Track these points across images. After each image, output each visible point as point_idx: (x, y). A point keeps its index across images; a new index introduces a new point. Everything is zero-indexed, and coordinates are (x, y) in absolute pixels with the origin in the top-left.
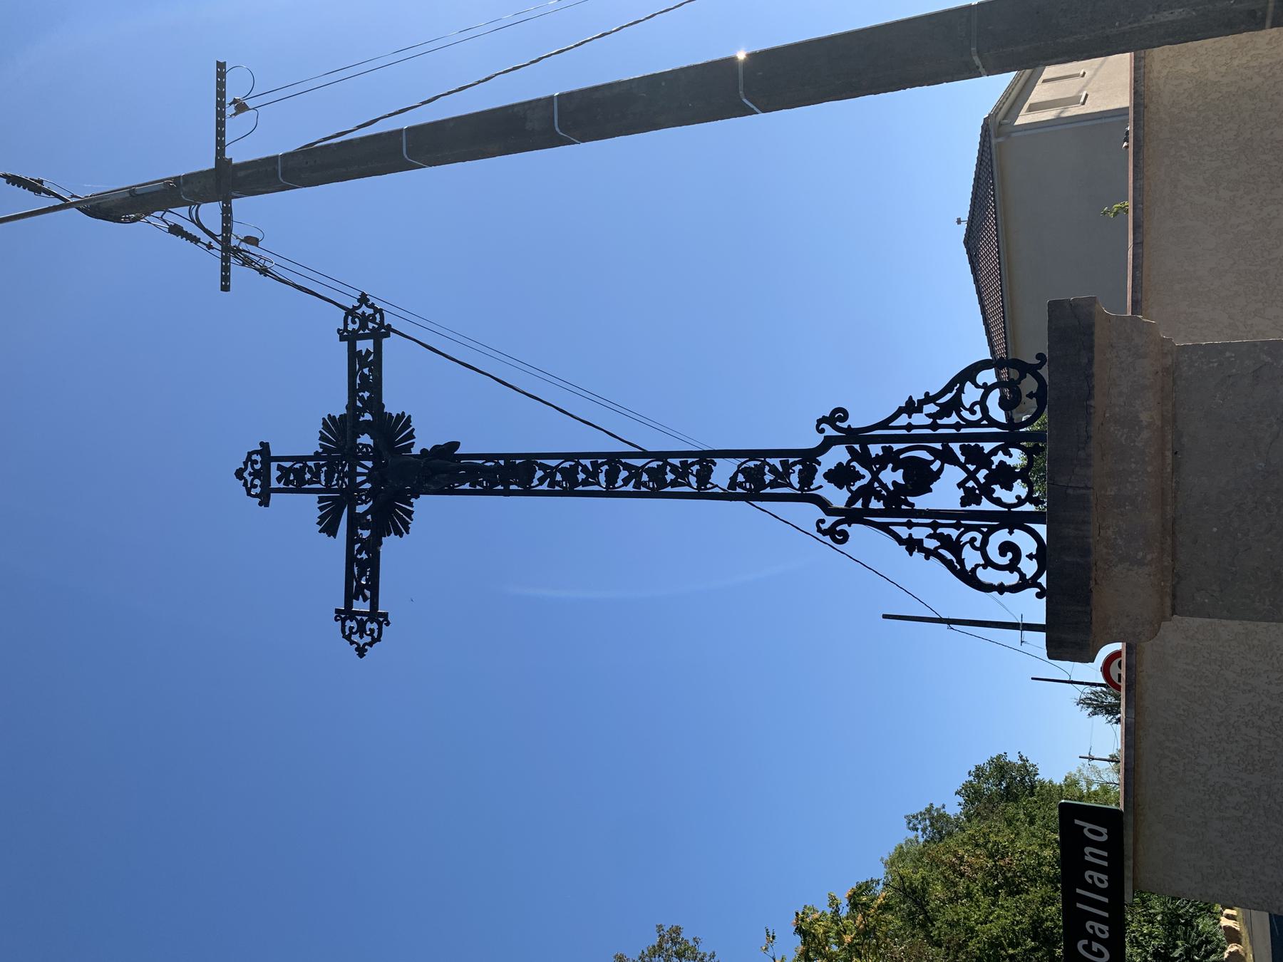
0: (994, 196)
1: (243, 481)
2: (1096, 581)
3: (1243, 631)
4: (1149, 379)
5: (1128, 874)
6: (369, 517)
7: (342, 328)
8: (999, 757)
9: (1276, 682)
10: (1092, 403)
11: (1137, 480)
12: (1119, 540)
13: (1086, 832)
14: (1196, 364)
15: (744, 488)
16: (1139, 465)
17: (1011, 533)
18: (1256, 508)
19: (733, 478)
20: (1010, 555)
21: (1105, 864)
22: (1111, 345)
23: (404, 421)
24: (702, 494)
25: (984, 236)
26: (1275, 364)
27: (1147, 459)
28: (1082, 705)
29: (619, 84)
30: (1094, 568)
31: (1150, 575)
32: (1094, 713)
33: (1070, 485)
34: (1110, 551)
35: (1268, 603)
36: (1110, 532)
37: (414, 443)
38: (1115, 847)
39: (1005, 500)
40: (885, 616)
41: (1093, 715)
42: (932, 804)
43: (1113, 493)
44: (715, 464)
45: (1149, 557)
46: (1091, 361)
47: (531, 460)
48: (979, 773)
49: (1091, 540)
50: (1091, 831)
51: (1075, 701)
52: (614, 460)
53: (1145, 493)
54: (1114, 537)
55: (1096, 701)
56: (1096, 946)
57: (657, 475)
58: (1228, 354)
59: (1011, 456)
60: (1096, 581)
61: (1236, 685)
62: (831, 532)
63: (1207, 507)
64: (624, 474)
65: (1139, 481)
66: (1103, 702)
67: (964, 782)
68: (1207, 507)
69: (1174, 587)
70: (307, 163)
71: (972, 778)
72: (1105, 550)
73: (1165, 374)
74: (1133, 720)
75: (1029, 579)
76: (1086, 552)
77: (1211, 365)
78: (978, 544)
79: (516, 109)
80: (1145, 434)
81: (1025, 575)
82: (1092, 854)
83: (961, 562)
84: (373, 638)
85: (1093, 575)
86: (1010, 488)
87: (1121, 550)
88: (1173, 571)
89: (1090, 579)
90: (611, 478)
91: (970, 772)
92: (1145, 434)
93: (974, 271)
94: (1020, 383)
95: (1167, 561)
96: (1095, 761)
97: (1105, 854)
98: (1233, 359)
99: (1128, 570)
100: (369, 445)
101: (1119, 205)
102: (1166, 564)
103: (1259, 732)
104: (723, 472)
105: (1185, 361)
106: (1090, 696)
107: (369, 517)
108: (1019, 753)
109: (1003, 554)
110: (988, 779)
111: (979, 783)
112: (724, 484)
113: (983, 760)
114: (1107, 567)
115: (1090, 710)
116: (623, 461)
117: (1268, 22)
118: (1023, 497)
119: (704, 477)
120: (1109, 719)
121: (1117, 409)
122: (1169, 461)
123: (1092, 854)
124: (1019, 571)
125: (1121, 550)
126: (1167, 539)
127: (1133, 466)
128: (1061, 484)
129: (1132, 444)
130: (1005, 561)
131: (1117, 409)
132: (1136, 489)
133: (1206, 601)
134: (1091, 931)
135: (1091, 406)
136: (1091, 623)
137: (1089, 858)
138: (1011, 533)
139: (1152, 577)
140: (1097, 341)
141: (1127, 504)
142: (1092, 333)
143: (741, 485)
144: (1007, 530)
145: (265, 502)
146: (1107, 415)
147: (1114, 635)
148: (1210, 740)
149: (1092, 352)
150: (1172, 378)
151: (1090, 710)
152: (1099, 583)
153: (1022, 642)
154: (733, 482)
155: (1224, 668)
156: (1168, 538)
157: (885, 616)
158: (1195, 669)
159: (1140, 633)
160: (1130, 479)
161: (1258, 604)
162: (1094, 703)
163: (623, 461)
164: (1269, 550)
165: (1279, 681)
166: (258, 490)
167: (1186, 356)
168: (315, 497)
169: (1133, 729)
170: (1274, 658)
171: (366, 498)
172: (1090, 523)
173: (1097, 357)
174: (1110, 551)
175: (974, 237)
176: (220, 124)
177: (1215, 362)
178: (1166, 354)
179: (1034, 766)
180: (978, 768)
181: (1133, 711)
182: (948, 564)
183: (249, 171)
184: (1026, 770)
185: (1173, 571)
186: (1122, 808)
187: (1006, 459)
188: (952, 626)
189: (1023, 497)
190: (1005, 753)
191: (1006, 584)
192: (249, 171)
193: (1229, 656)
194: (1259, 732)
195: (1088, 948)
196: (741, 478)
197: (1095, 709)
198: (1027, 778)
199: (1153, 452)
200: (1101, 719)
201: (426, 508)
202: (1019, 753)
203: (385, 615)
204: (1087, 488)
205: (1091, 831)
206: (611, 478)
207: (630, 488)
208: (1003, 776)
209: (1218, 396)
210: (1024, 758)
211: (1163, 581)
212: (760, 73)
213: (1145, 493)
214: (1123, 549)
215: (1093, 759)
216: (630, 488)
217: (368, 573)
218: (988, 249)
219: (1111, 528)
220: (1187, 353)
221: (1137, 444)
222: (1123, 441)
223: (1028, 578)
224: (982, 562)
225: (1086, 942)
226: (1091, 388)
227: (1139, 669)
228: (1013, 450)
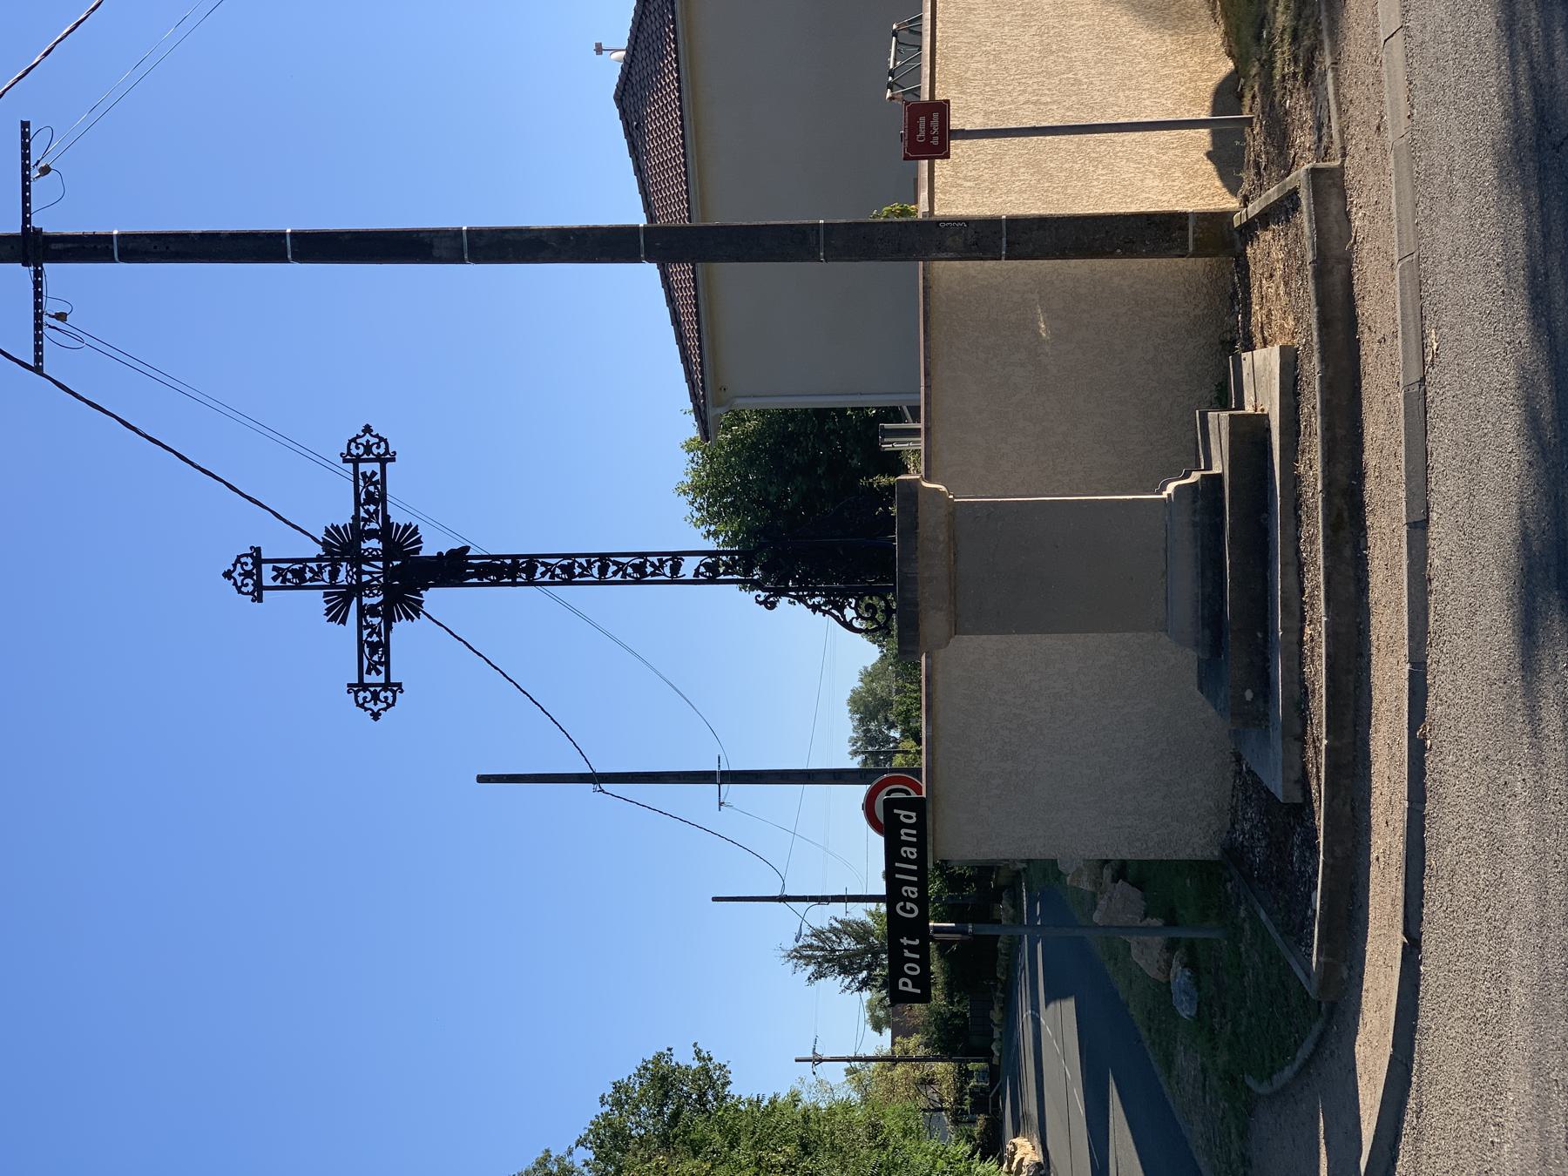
0: (675, 41)
1: (232, 580)
5: (930, 847)
6: (380, 608)
7: (345, 452)
8: (659, 1057)
10: (918, 531)
13: (902, 818)
15: (705, 576)
19: (697, 570)
21: (915, 840)
23: (412, 531)
24: (675, 580)
28: (795, 961)
29: (528, 230)
32: (819, 975)
37: (421, 547)
38: (921, 826)
40: (483, 779)
41: (817, 978)
42: (547, 1151)
44: (683, 560)
47: (532, 560)
48: (620, 1097)
50: (906, 816)
51: (783, 954)
52: (604, 558)
55: (822, 949)
56: (909, 905)
57: (639, 569)
62: (764, 603)
64: (613, 568)
66: (833, 950)
67: (594, 1119)
69: (956, 621)
70: (155, 247)
71: (607, 1108)
76: (917, 605)
78: (853, 605)
79: (421, 235)
80: (941, 546)
82: (906, 834)
83: (844, 616)
84: (388, 704)
90: (603, 570)
91: (603, 1097)
92: (941, 546)
93: (635, 150)
96: (824, 1063)
97: (914, 832)
100: (379, 549)
101: (889, 208)
104: (689, 567)
106: (810, 940)
107: (380, 608)
108: (695, 1045)
110: (637, 1107)
111: (621, 1115)
112: (690, 576)
113: (626, 1067)
115: (811, 968)
116: (612, 559)
117: (1003, 258)
119: (675, 569)
120: (847, 981)
123: (906, 834)
134: (905, 894)
137: (904, 838)
143: (702, 574)
145: (259, 599)
151: (811, 968)
153: (721, 804)
154: (697, 573)
157: (483, 779)
162: (818, 953)
163: (612, 559)
166: (250, 588)
168: (321, 592)
171: (379, 592)
176: (26, 189)
179: (722, 1067)
180: (617, 1087)
182: (836, 618)
183: (69, 245)
184: (709, 1079)
186: (924, 795)
188: (604, 786)
190: (669, 1049)
192: (69, 245)
195: (903, 909)
196: (702, 569)
197: (820, 965)
198: (710, 1092)
200: (834, 983)
201: (433, 598)
202: (695, 1045)
203: (399, 685)
205: (906, 816)
206: (603, 570)
207: (547, 578)
208: (666, 1095)
210: (704, 1054)
212: (658, 244)
215: (821, 1061)
216: (547, 578)
217: (380, 653)
224: (855, 616)
225: (902, 904)
226: (917, 523)
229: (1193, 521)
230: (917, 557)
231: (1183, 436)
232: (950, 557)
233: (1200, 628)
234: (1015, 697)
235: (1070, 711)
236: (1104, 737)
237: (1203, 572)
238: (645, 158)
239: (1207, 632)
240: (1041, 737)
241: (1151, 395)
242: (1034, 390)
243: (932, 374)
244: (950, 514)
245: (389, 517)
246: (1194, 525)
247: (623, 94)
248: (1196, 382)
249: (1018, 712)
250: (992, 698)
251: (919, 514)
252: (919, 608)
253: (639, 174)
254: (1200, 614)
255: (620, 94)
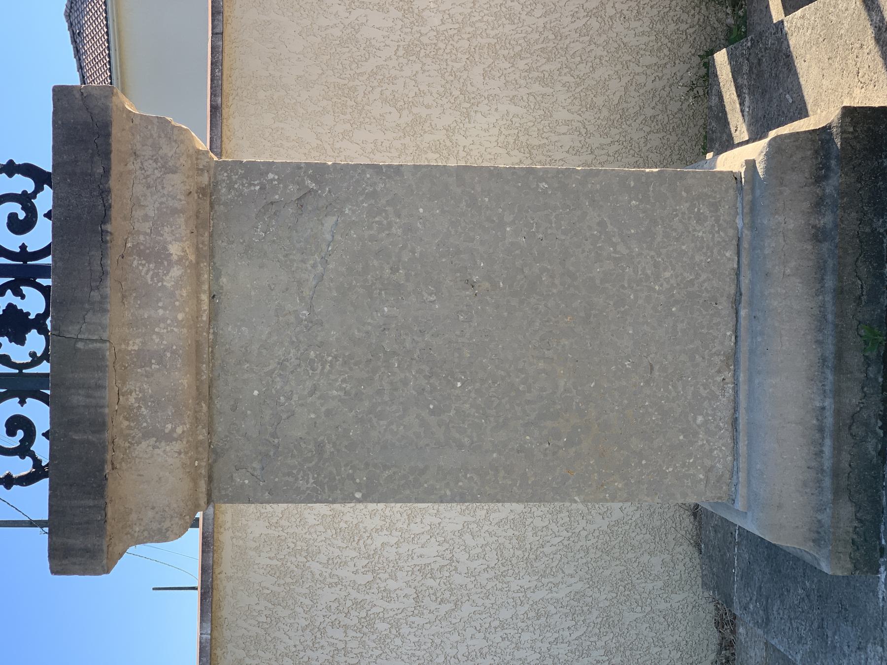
2: (113, 464)
3: (331, 513)
4: (180, 200)
9: (363, 570)
10: (108, 227)
11: (165, 330)
12: (143, 409)
14: (236, 186)
16: (168, 312)
17: (22, 402)
18: (299, 365)
20: (20, 434)
22: (135, 153)
25: (93, 7)
26: (320, 192)
27: (177, 303)
30: (110, 447)
31: (180, 453)
33: (80, 337)
34: (132, 424)
35: (311, 481)
36: (132, 400)
39: (15, 359)
43: (136, 348)
45: (179, 430)
46: (107, 172)
49: (107, 410)
53: (174, 347)
54: (137, 405)
58: (271, 176)
59: (23, 297)
60: (113, 464)
61: (321, 579)
63: (248, 365)
65: (168, 332)
68: (248, 365)
69: (210, 468)
72: (126, 423)
73: (201, 196)
74: (209, 636)
75: (45, 466)
76: (100, 425)
77: (252, 188)
80: (176, 272)
81: (40, 461)
85: (108, 457)
86: (21, 341)
87: (146, 422)
88: (210, 446)
89: (103, 462)
94: (35, 197)
95: (202, 435)
98: (276, 183)
99: (154, 447)
102: (201, 437)
103: (345, 632)
105: (224, 181)
109: (11, 432)
114: (127, 445)
118: (39, 355)
121: (142, 238)
122: (205, 307)
124: (33, 456)
125: (146, 422)
126: (202, 407)
127: (161, 312)
128: (68, 336)
129: (160, 284)
130: (14, 442)
131: (142, 238)
132: (165, 342)
133: (247, 482)
135: (107, 232)
136: (106, 521)
138: (22, 402)
139: (182, 456)
140: (115, 146)
141: (153, 361)
142: (108, 135)
144: (17, 399)
146: (129, 245)
147: (136, 535)
148: (294, 649)
149: (109, 159)
150: (208, 202)
152: (118, 466)
155: (310, 559)
156: (204, 405)
158: (279, 564)
159: (167, 530)
160: (157, 330)
161: (301, 482)
164: (313, 416)
165: (366, 569)
167: (225, 174)
169: (208, 648)
170: (361, 542)
172: (105, 388)
173: (116, 169)
174: (132, 424)
175: (78, 9)
177: (258, 185)
178: (202, 170)
181: (210, 624)
185: (210, 446)
187: (17, 301)
189: (39, 355)
191: (15, 475)
193: (316, 544)
194: (345, 632)
199: (185, 295)
204: (103, 341)
209: (260, 227)
211: (197, 459)
213: (174, 347)
214: (149, 420)
218: (93, 27)
219: (134, 394)
220: (226, 172)
221: (165, 283)
222: (149, 280)
223: (43, 464)
226: (107, 208)
227: (217, 571)
228: (25, 289)
229: (814, 227)
230: (104, 297)
231: (643, 140)
232: (199, 301)
233: (829, 496)
234: (355, 573)
235: (447, 594)
236: (503, 639)
237: (839, 355)
238: (84, 57)
239: (847, 510)
240: (398, 641)
241: (594, 69)
242: (401, 52)
243: (226, 14)
244: (202, 191)
245: (39, 333)
246: (819, 236)
247: (71, 12)
248: (666, 52)
249: (360, 597)
250: (317, 573)
251: (113, 183)
252: (107, 435)
253: (80, 70)
254: (827, 464)
255: (68, 11)
